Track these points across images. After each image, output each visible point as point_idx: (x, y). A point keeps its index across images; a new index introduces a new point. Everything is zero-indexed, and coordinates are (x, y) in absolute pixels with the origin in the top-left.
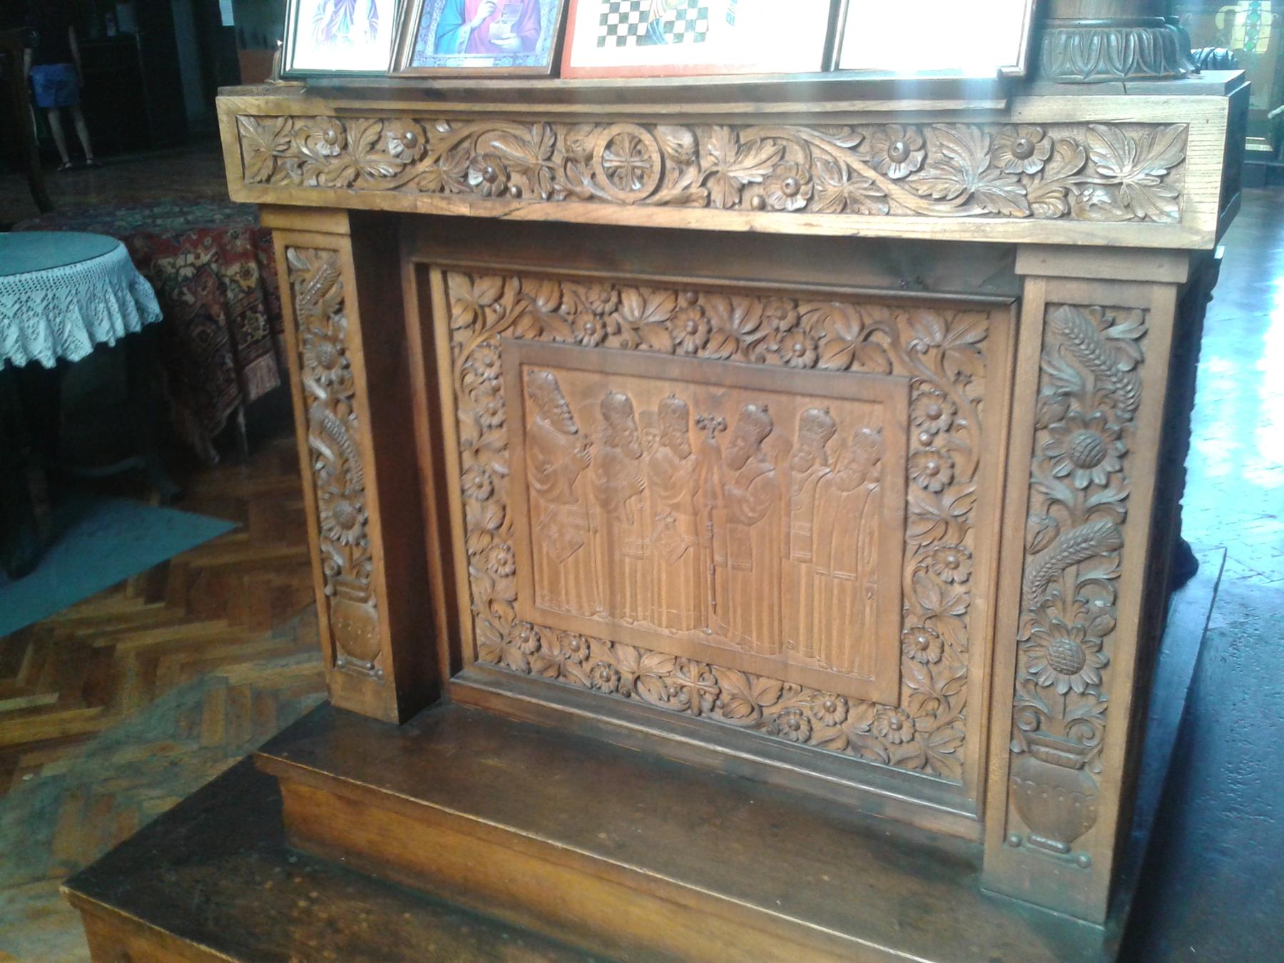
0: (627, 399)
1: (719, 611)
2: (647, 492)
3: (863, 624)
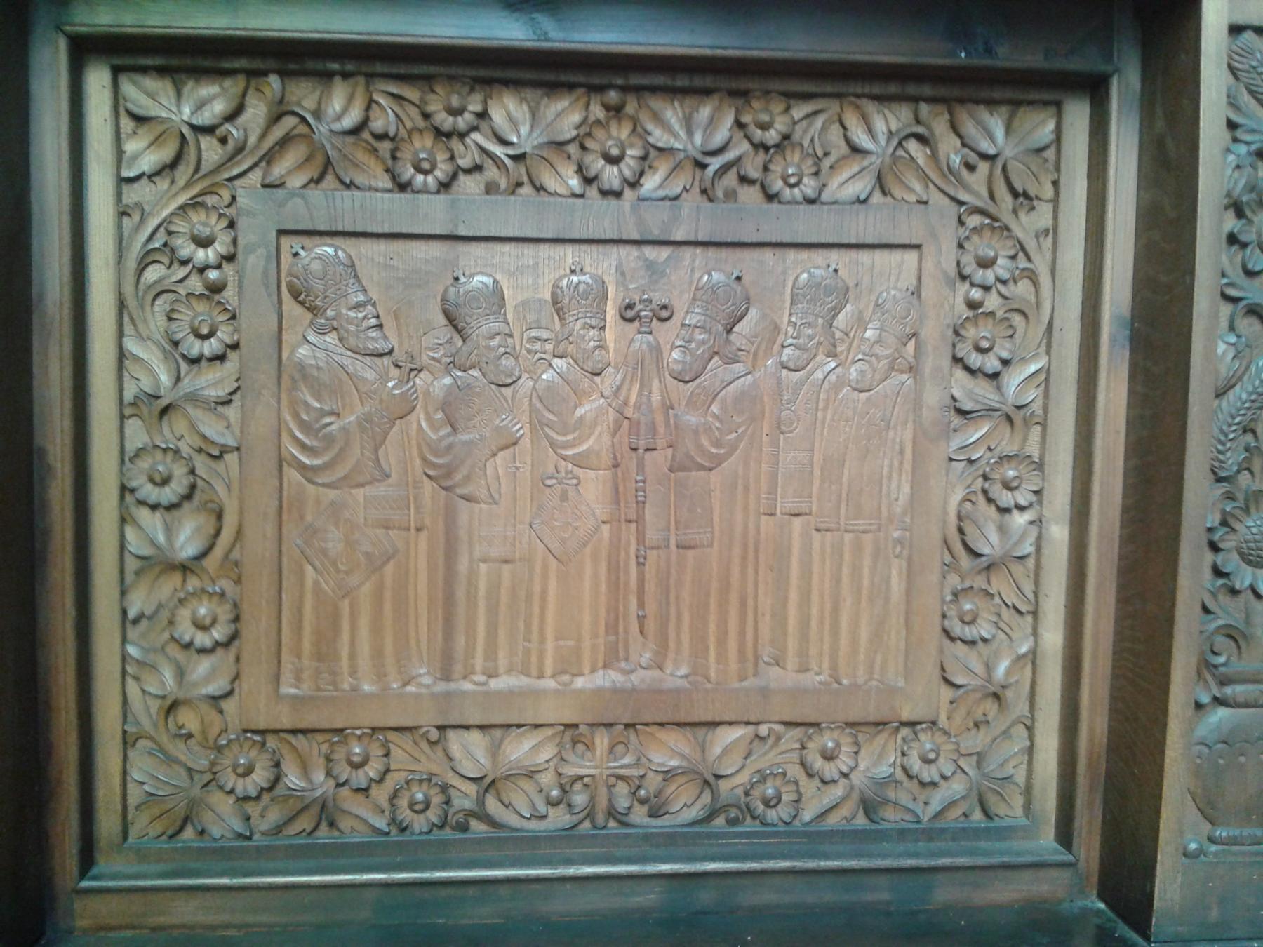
0: (496, 282)
1: (651, 626)
2: (526, 443)
3: (887, 599)
